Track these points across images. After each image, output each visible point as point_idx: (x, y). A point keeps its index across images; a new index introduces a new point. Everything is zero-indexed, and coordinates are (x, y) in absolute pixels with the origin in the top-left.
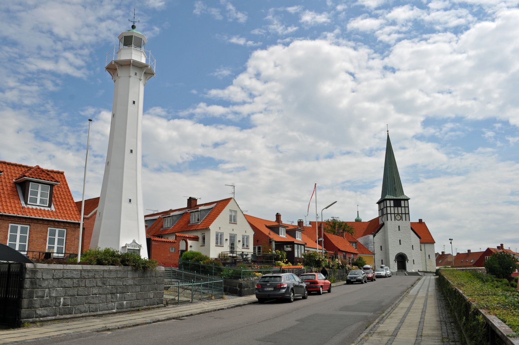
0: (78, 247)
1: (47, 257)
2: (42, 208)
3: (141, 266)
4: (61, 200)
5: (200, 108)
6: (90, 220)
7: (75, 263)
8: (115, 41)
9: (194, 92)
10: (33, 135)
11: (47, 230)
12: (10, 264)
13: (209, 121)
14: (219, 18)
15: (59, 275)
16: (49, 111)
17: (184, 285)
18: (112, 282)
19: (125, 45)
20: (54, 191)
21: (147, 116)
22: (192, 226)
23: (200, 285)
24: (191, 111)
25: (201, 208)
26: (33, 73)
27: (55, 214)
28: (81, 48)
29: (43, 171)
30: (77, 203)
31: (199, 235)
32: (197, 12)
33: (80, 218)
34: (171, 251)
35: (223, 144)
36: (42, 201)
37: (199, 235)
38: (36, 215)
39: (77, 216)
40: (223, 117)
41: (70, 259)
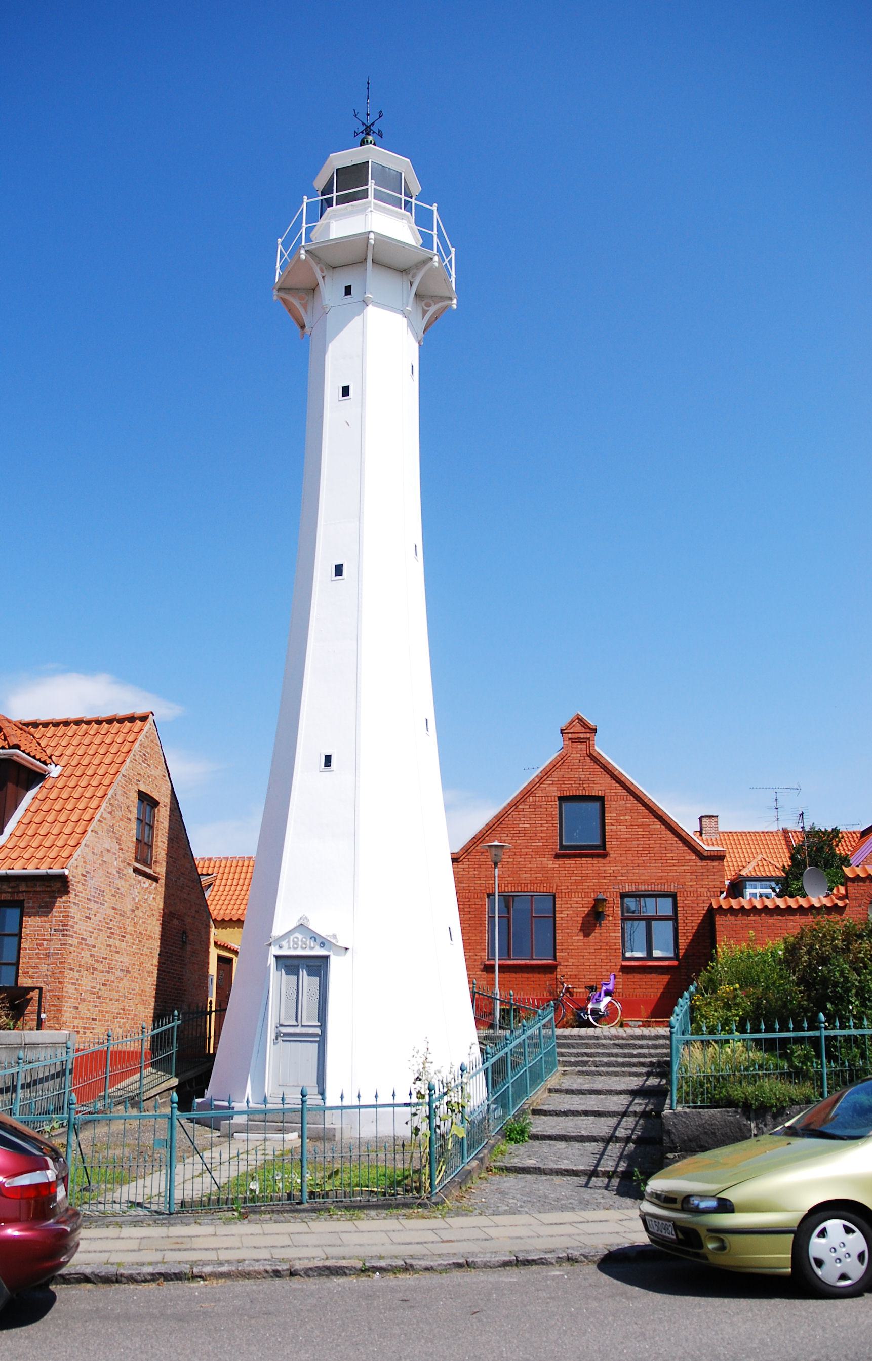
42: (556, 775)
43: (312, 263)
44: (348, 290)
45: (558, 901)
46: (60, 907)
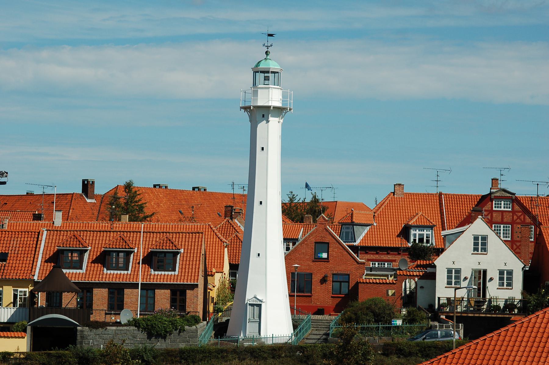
42: (314, 235)
44: (263, 116)
45: (313, 276)
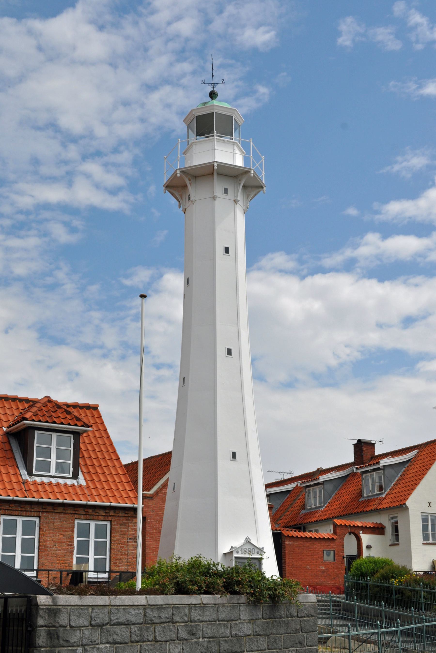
0: (135, 557)
1: (76, 581)
2: (61, 481)
3: (267, 593)
4: (96, 464)
5: (366, 244)
6: (156, 500)
7: (132, 591)
8: (180, 127)
9: (352, 212)
10: (34, 335)
11: (74, 526)
12: (6, 598)
13: (389, 271)
14: (394, 46)
15: (102, 617)
16: (63, 285)
17: (360, 632)
18: (209, 631)
19: (199, 133)
20: (82, 446)
21: (255, 274)
22: (368, 501)
23: (394, 633)
24: (348, 253)
25: (384, 462)
26: (27, 213)
27: (86, 491)
28: (116, 151)
29: (58, 406)
30: (127, 466)
31: (385, 520)
32: (345, 41)
33: (136, 498)
34: (326, 558)
35: (424, 317)
36: (60, 467)
37: (385, 520)
38: (51, 495)
39: (131, 494)
40: (419, 259)
41: (122, 584)
43: (184, 177)
46: (132, 526)
